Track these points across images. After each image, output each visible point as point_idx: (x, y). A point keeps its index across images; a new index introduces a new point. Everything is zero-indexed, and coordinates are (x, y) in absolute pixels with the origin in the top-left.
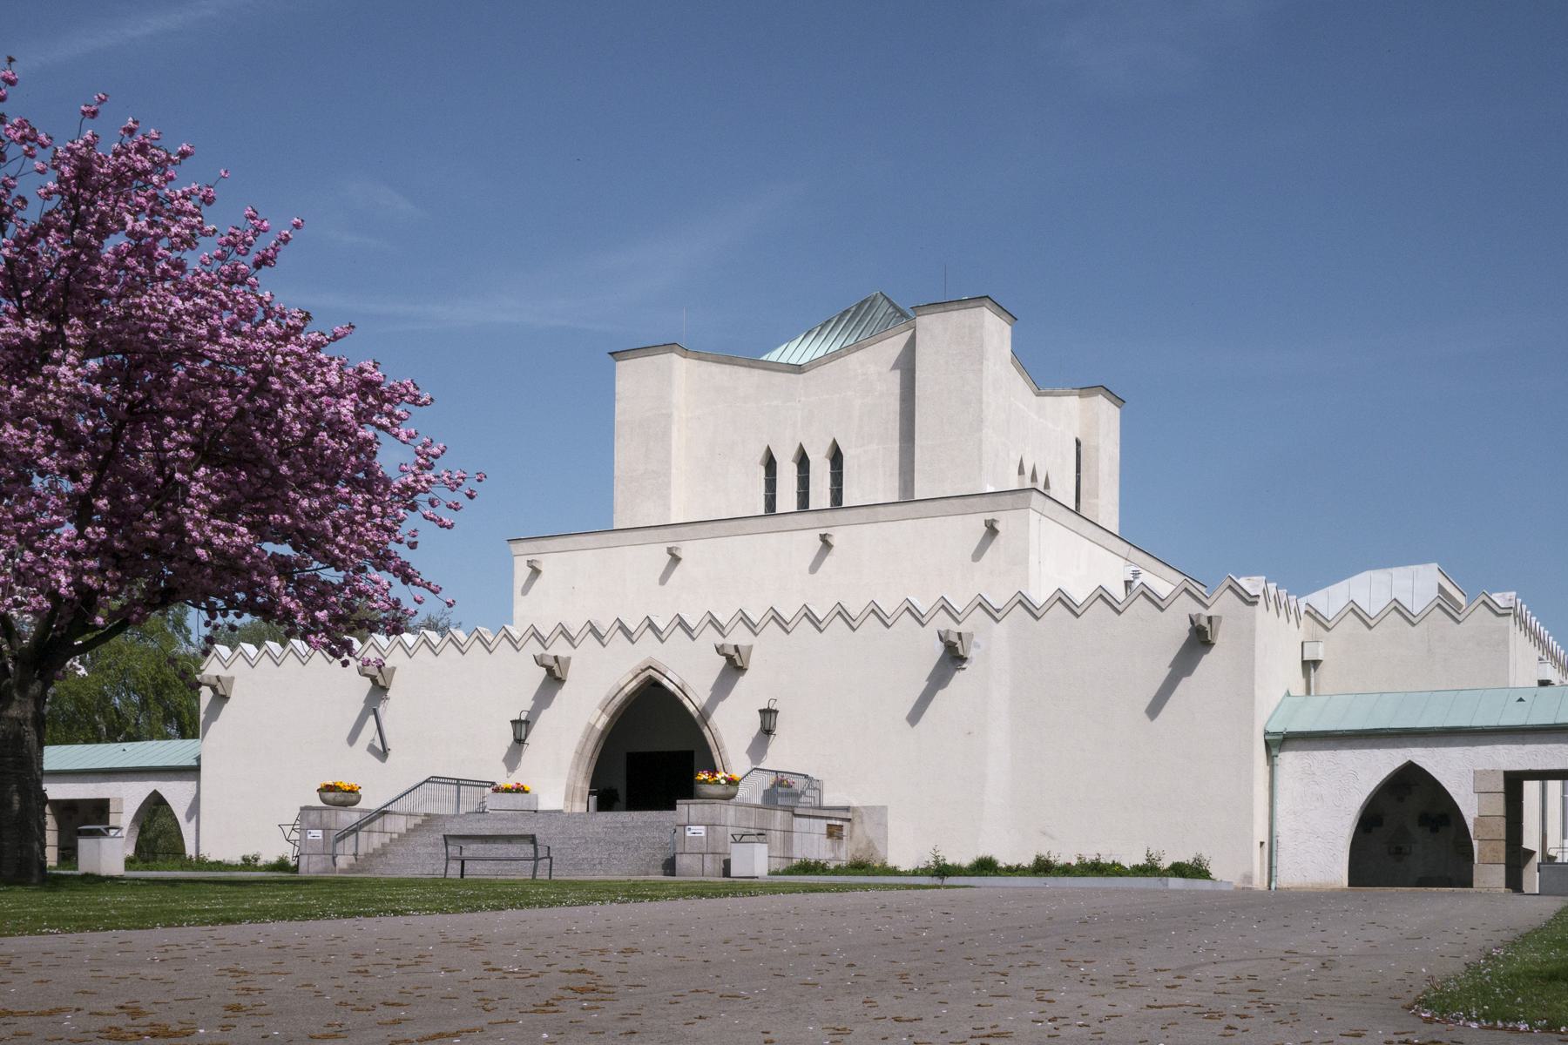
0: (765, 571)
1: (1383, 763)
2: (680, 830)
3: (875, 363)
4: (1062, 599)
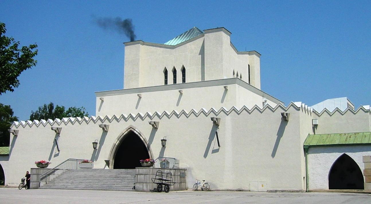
0: (165, 101)
1: (334, 156)
2: (136, 176)
3: (195, 46)
4: (245, 109)
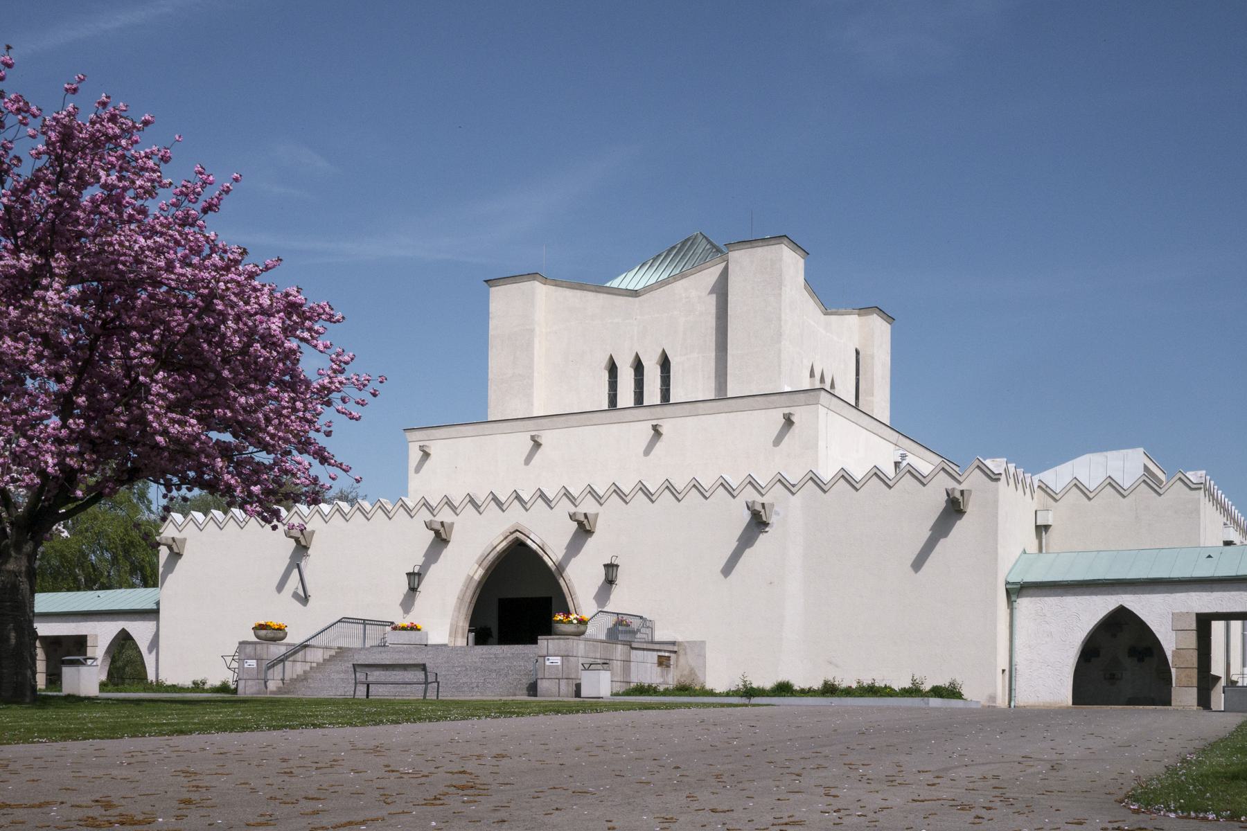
0: (608, 454)
1: (1100, 607)
2: (540, 660)
3: (696, 289)
4: (845, 476)
